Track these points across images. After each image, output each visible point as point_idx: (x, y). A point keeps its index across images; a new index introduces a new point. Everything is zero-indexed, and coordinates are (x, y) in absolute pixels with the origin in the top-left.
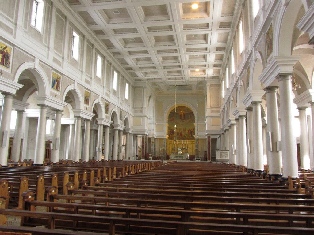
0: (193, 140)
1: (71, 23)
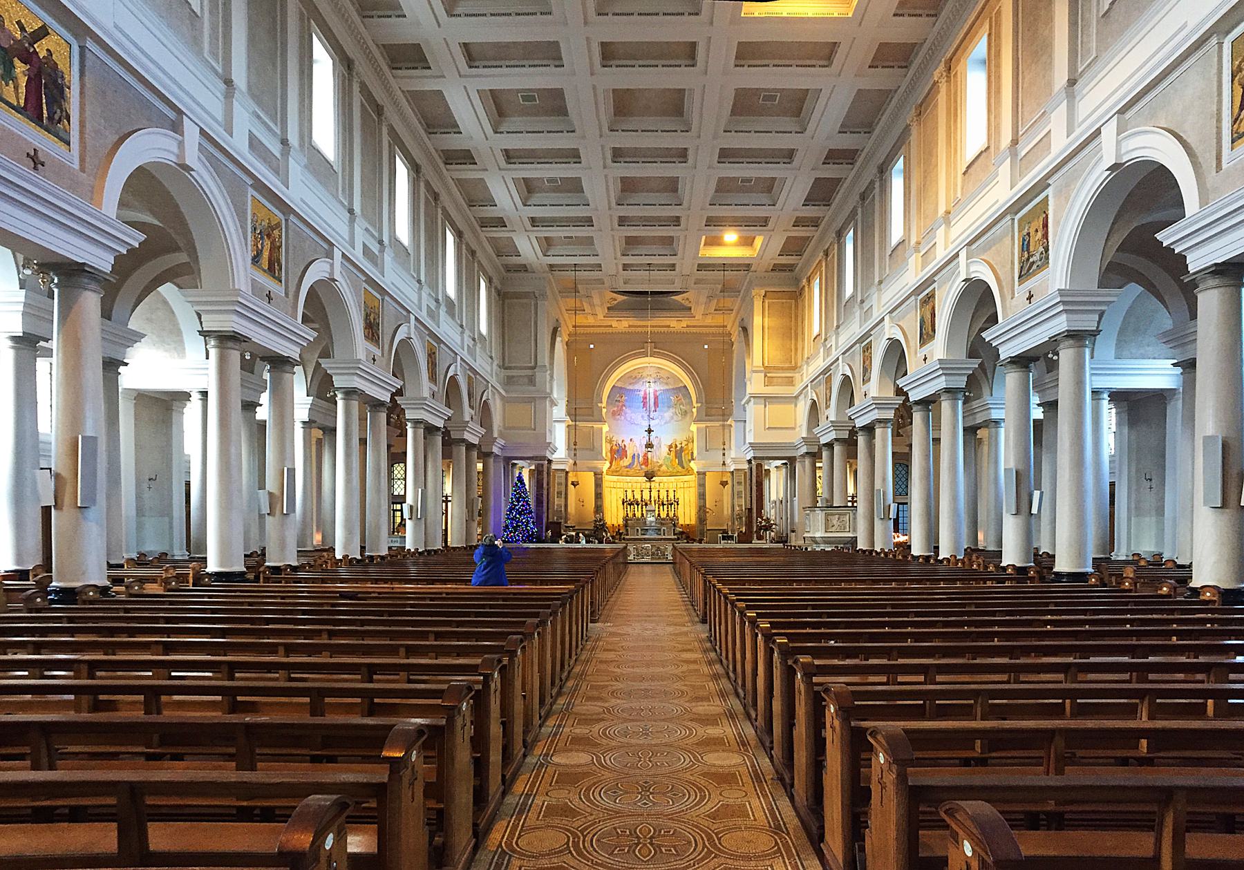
0: (686, 478)
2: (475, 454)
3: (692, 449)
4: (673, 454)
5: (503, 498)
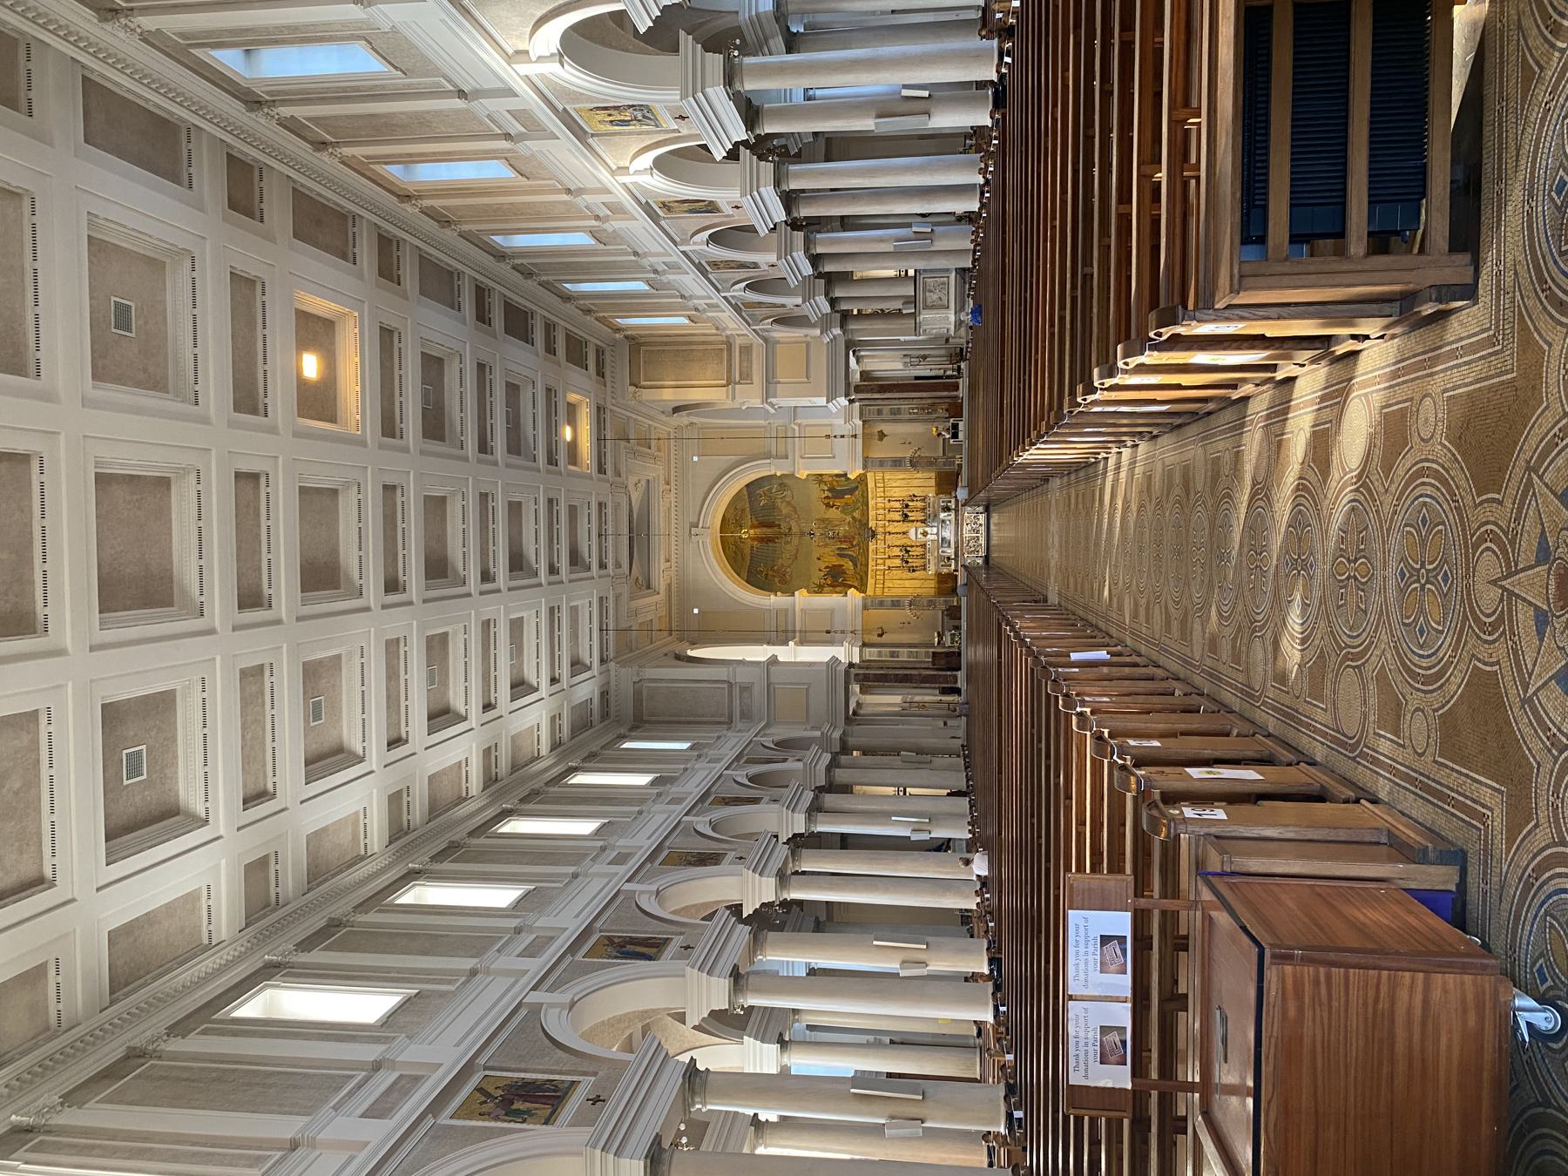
0: (871, 485)
1: (364, 906)
2: (843, 759)
3: (831, 476)
4: (838, 503)
5: (901, 726)
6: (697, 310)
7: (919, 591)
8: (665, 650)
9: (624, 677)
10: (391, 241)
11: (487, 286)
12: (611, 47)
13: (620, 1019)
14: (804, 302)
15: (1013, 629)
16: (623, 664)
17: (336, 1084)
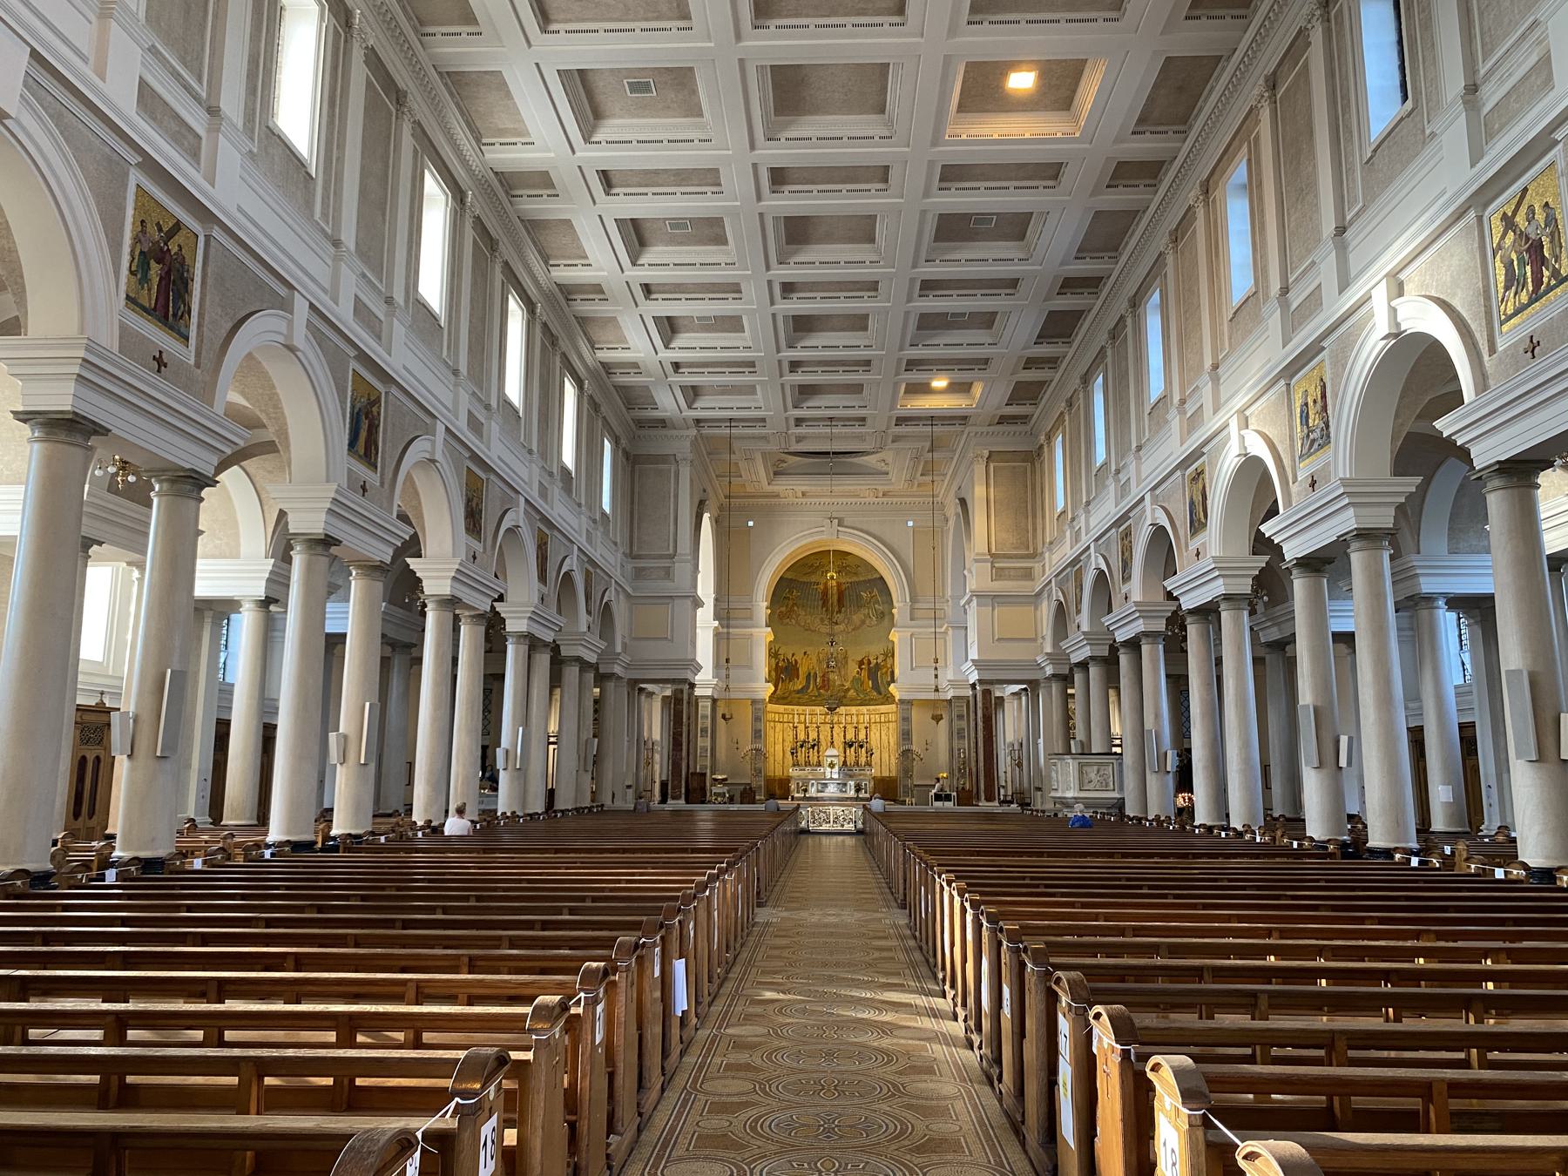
0: (883, 708)
1: (420, 132)
2: (590, 676)
4: (864, 674)
5: (626, 738)
6: (1073, 519)
7: (772, 759)
8: (709, 490)
9: (681, 445)
10: (1156, 177)
11: (1101, 291)
12: (1401, 397)
13: (277, 406)
14: (1084, 633)
15: (722, 872)
16: (694, 443)
17: (192, 60)
